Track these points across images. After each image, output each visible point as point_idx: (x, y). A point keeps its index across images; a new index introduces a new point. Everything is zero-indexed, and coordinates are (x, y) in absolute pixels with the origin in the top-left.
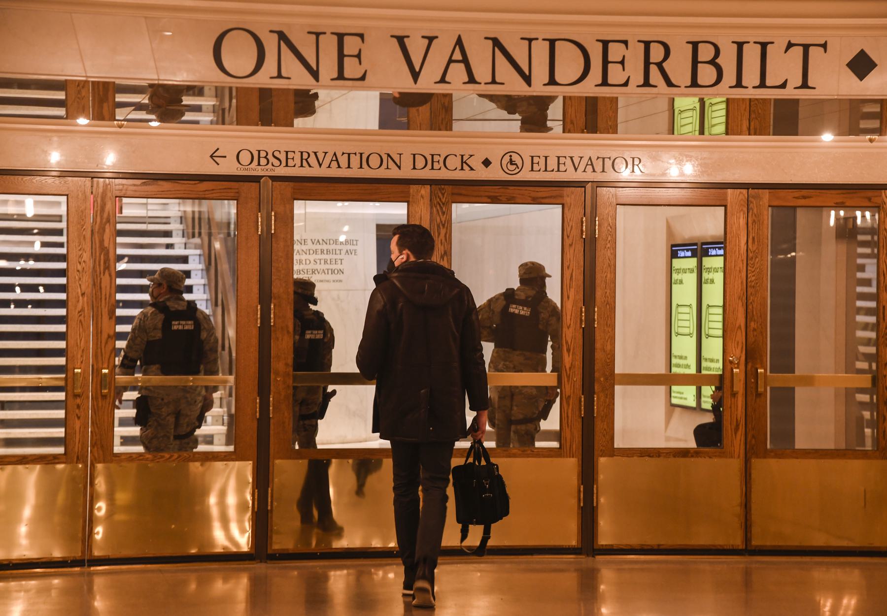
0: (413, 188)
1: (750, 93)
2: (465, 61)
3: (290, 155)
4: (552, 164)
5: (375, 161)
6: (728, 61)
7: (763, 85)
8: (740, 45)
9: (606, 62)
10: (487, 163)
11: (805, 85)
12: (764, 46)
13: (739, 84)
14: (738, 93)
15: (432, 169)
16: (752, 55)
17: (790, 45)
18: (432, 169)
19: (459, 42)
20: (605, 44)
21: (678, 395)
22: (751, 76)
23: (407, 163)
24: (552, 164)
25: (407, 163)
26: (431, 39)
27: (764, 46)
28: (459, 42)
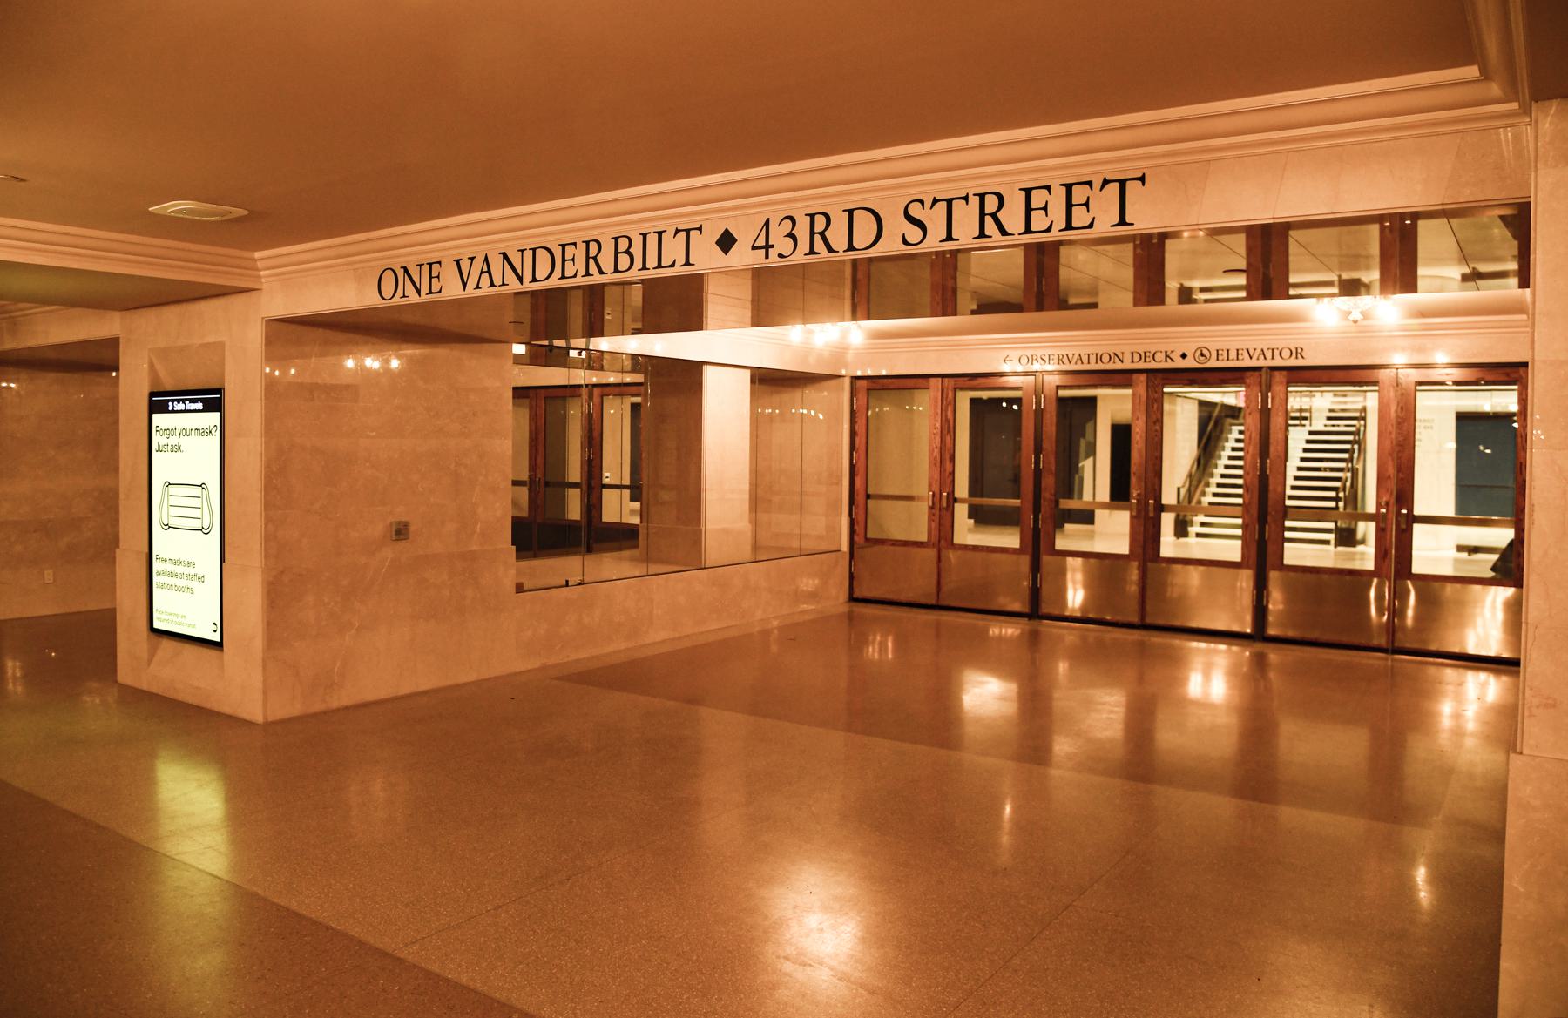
0: (1135, 376)
2: (489, 271)
4: (1233, 355)
5: (1105, 358)
6: (637, 250)
7: (659, 266)
8: (645, 235)
9: (564, 260)
11: (687, 263)
12: (660, 234)
13: (644, 268)
14: (645, 275)
16: (652, 241)
17: (677, 231)
19: (486, 259)
22: (652, 261)
23: (1127, 358)
24: (1233, 355)
25: (1127, 358)
26: (472, 259)
28: (486, 259)
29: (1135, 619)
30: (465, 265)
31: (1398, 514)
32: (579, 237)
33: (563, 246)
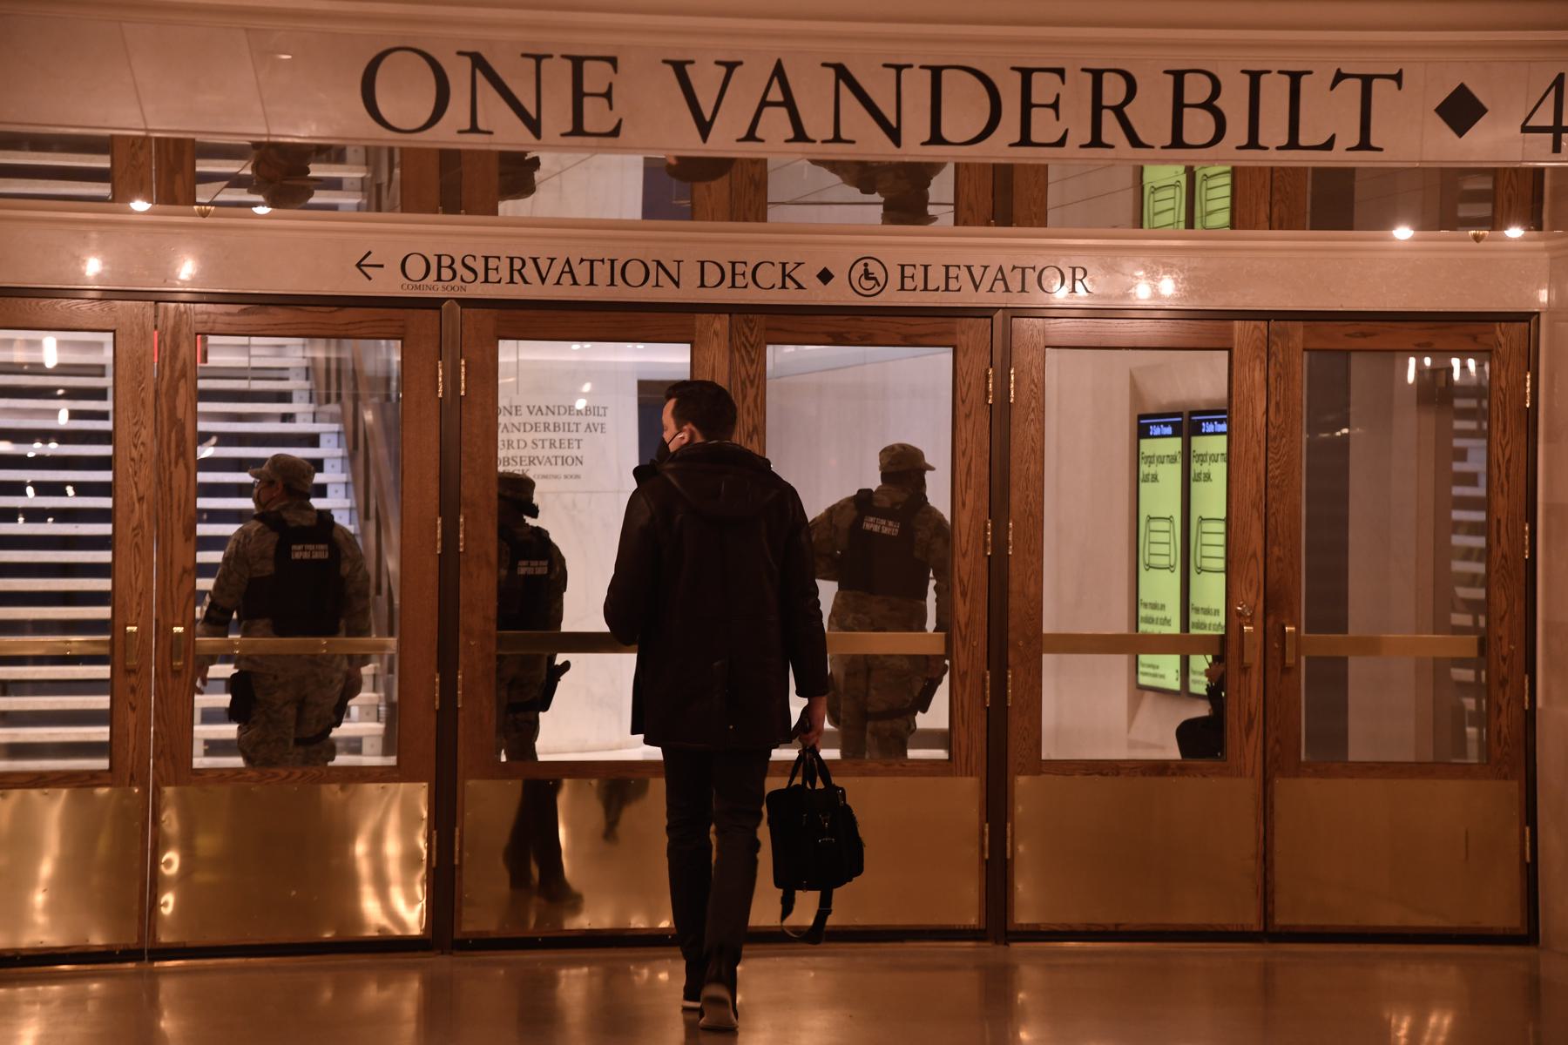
0: (701, 320)
1: (1272, 157)
2: (789, 103)
3: (492, 263)
4: (937, 278)
5: (636, 272)
6: (1234, 104)
7: (1293, 143)
8: (1255, 77)
9: (1027, 106)
11: (1365, 144)
12: (1295, 78)
13: (1253, 143)
15: (733, 286)
17: (1340, 77)
18: (733, 286)
19: (779, 72)
22: (1274, 129)
23: (690, 276)
24: (937, 278)
25: (690, 276)
27: (1295, 78)
28: (779, 72)
29: (1252, 921)
30: (706, 82)
31: (164, 630)
32: (1075, 60)
33: (1026, 74)
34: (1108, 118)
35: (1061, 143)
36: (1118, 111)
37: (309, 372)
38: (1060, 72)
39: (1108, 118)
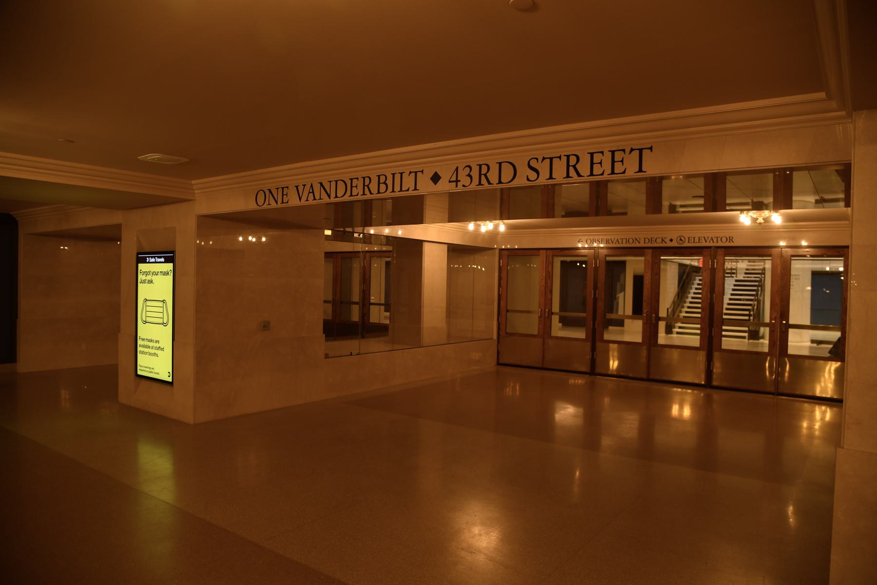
0: (646, 250)
1: (397, 194)
2: (313, 192)
4: (697, 240)
5: (631, 241)
8: (394, 174)
9: (352, 187)
10: (671, 240)
11: (415, 189)
12: (401, 174)
13: (393, 191)
17: (411, 172)
20: (352, 180)
21: (146, 343)
22: (397, 188)
24: (697, 240)
25: (642, 241)
27: (401, 174)
30: (301, 188)
32: (360, 175)
34: (571, 169)
35: (602, 174)
36: (574, 167)
37: (620, 323)
38: (602, 153)
39: (571, 169)
